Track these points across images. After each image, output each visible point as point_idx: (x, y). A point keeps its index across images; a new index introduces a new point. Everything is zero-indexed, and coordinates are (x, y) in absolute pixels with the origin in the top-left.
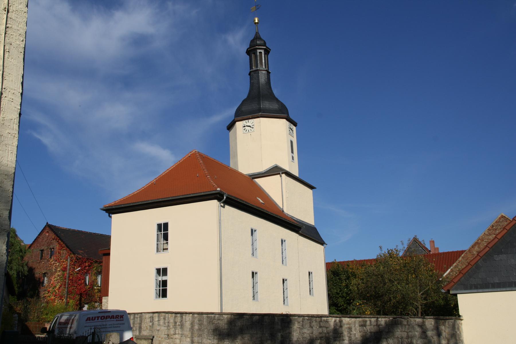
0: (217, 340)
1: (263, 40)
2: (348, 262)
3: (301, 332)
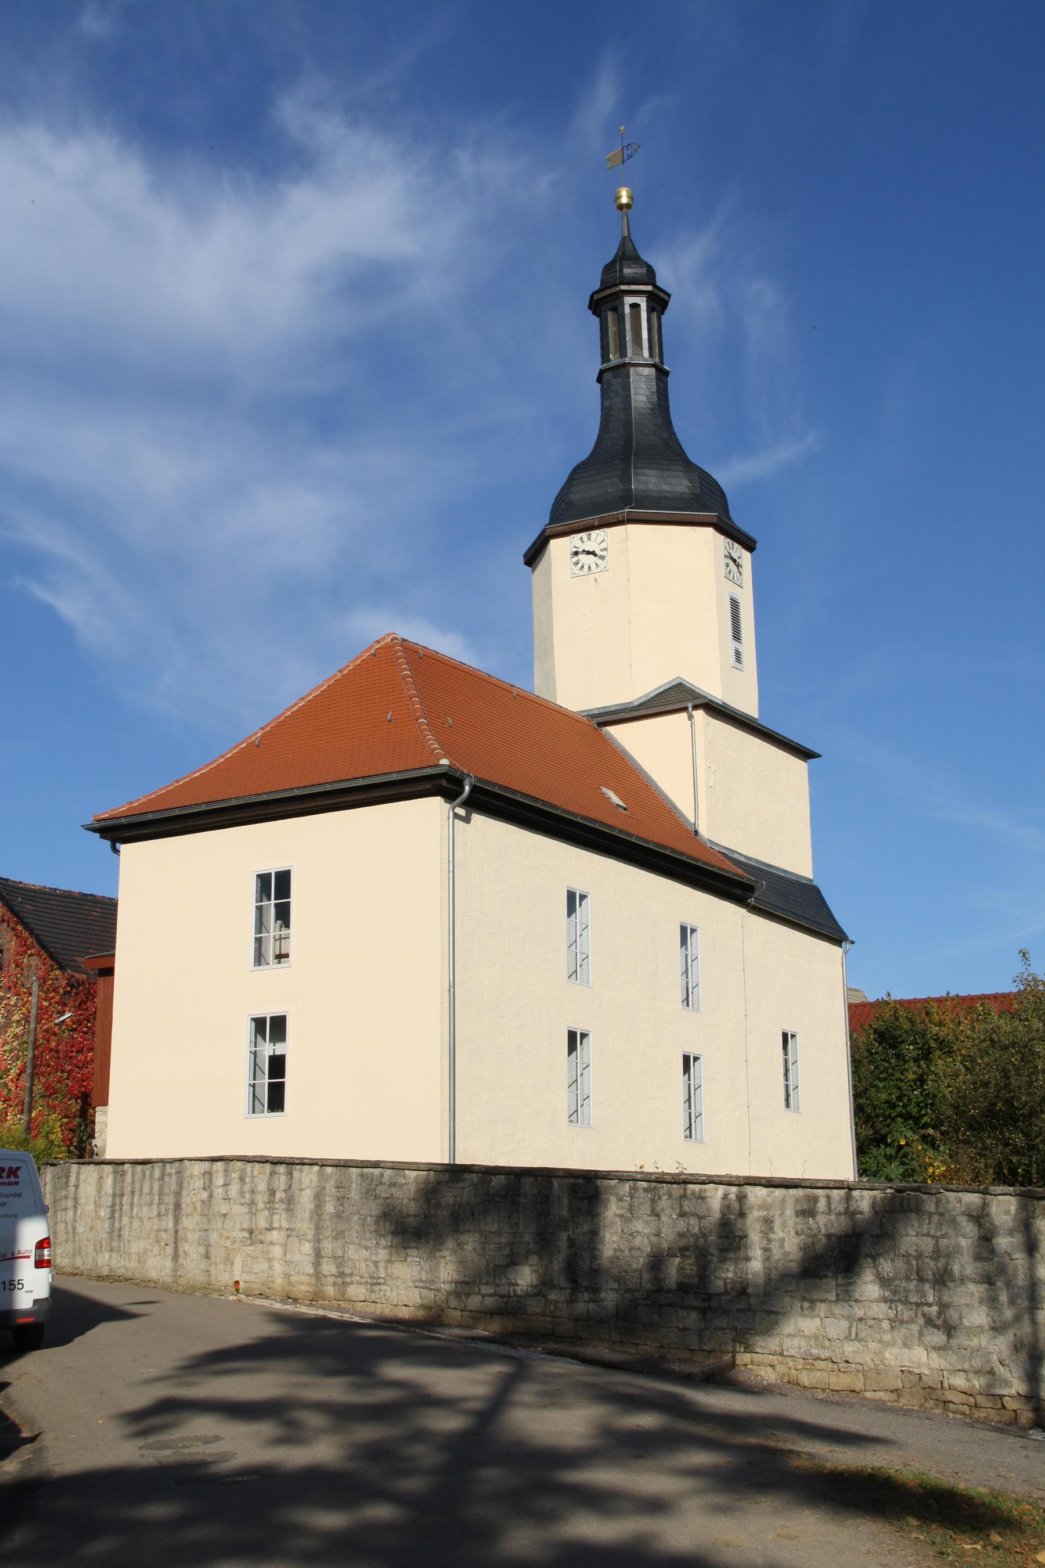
0: (387, 1251)
1: (646, 263)
2: (926, 1001)
3: (626, 1230)
